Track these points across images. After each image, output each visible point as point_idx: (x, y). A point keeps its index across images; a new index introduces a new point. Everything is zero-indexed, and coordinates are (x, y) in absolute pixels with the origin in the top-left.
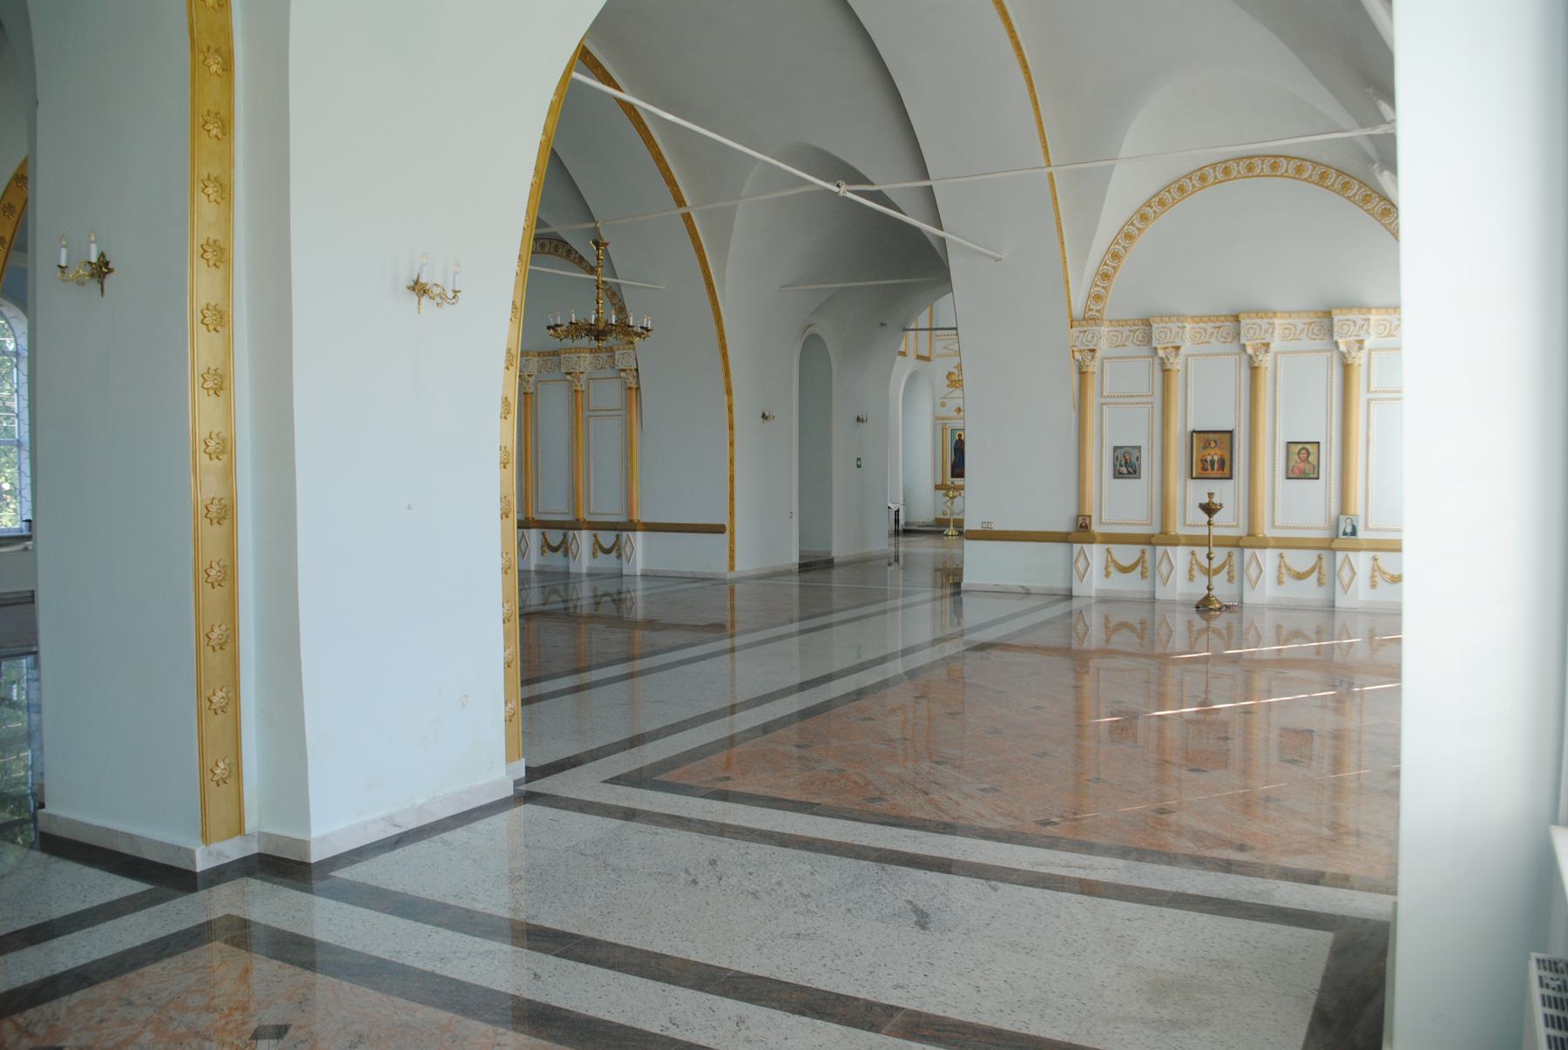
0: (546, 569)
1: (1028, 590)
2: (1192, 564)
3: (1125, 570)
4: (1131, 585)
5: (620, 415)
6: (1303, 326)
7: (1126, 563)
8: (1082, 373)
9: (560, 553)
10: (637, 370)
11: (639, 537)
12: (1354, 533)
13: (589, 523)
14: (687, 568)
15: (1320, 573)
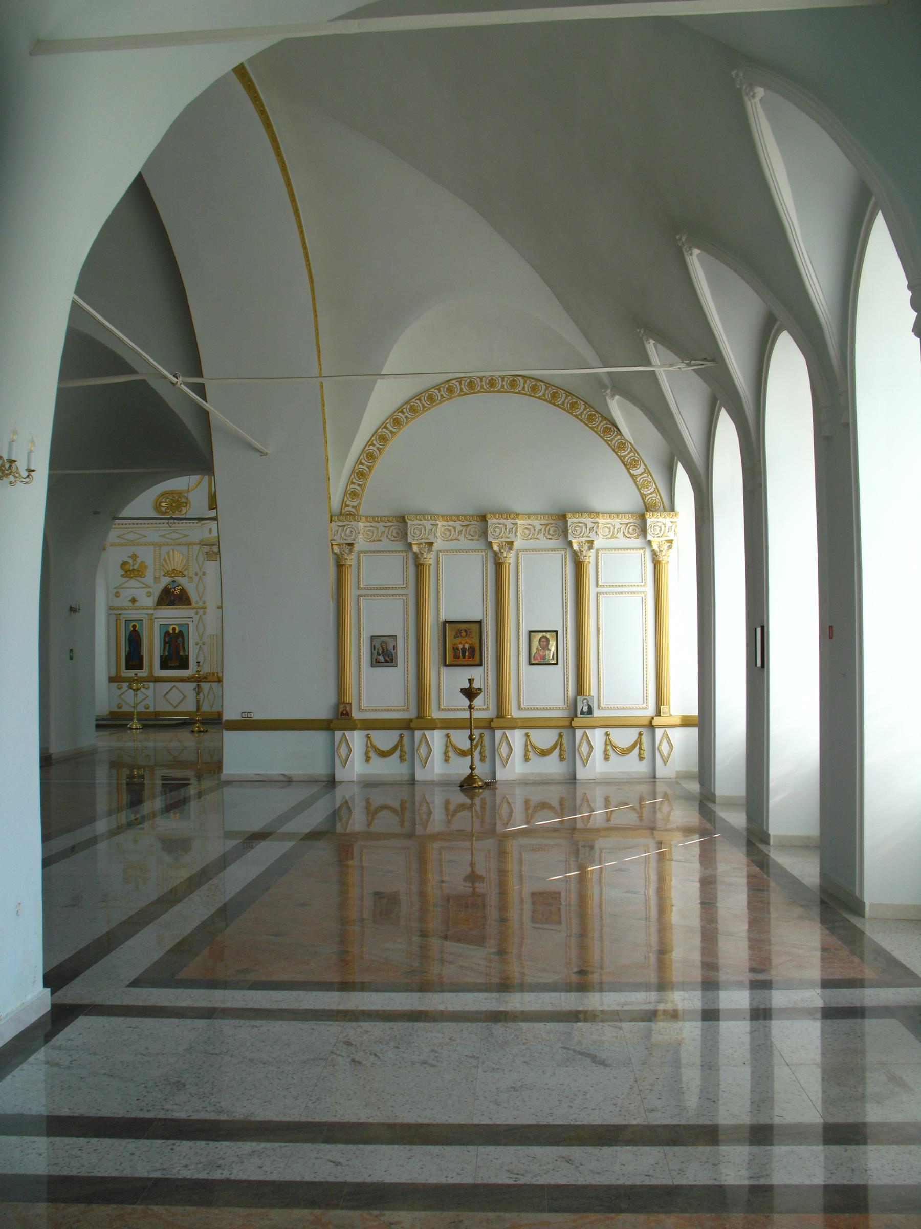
1: (290, 778)
3: (383, 754)
4: (390, 768)
6: (541, 527)
7: (385, 747)
8: (340, 567)
12: (590, 711)
15: (640, 749)
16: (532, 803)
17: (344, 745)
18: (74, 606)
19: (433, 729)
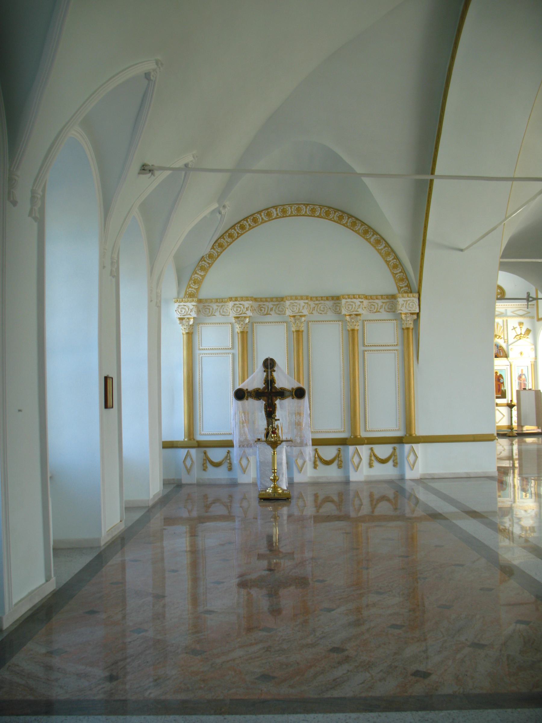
0: (320, 480)
2: (315, 458)
3: (383, 461)
5: (396, 350)
7: (328, 458)
9: (334, 465)
10: (418, 314)
11: (419, 448)
13: (368, 439)
14: (462, 470)
16: (376, 497)
17: (356, 456)
18: (522, 354)
19: (363, 444)
